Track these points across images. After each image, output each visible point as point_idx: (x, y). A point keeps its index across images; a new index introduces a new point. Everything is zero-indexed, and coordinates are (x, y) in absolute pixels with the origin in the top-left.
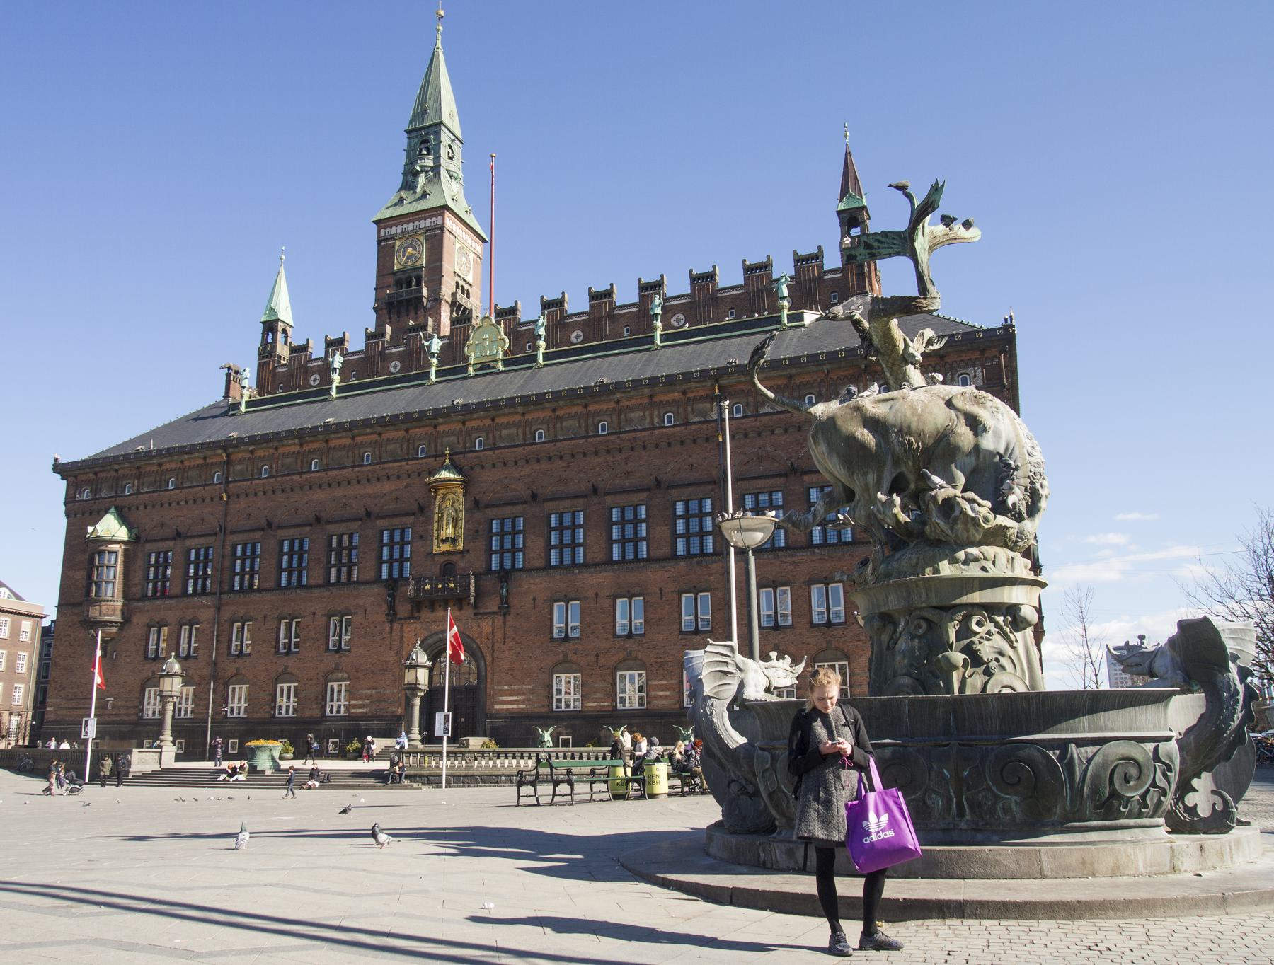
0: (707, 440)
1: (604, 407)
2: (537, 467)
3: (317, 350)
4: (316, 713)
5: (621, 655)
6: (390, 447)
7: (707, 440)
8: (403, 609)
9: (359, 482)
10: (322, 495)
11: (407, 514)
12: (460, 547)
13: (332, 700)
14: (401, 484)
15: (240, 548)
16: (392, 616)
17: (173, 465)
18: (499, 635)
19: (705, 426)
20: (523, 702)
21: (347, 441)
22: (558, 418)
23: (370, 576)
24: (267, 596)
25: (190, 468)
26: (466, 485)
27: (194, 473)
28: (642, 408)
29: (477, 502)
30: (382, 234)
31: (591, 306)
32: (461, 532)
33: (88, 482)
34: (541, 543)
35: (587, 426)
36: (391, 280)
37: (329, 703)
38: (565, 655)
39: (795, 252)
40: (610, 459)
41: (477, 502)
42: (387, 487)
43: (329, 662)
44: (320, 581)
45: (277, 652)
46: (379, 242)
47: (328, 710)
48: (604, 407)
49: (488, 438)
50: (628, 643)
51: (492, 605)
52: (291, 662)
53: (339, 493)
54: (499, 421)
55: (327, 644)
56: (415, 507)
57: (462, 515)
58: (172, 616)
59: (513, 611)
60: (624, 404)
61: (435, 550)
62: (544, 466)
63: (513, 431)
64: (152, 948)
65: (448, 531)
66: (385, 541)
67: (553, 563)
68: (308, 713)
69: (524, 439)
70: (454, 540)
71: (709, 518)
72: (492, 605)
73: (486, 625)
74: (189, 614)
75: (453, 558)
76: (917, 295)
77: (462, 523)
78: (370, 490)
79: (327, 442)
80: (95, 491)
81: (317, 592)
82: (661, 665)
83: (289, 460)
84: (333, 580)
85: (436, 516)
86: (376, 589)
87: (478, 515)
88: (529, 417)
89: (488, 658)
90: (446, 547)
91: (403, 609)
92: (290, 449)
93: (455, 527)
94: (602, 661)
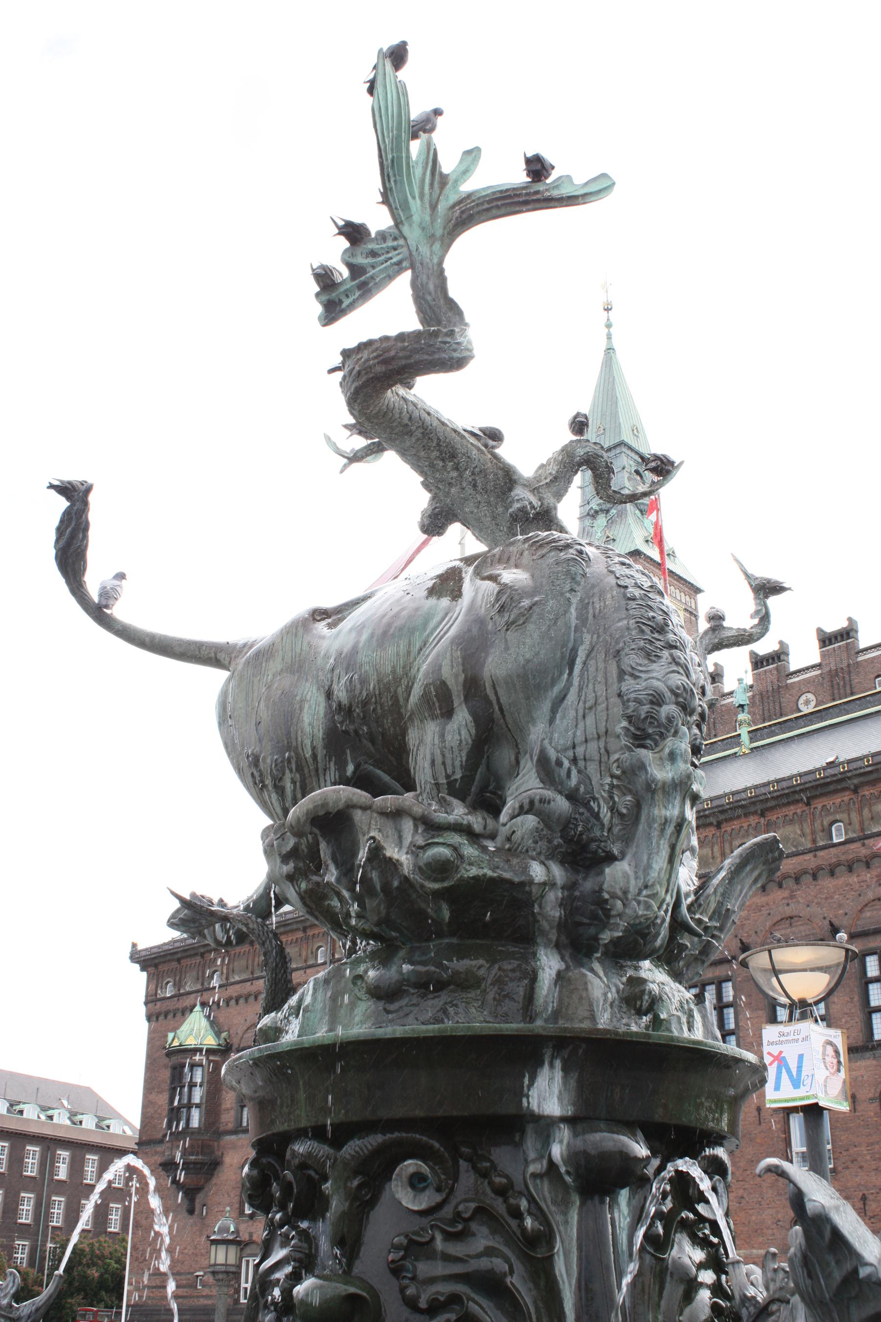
31: (823, 655)
35: (813, 832)
39: (820, 631)
40: (853, 879)
69: (814, 841)
71: (731, 1010)
76: (420, 327)
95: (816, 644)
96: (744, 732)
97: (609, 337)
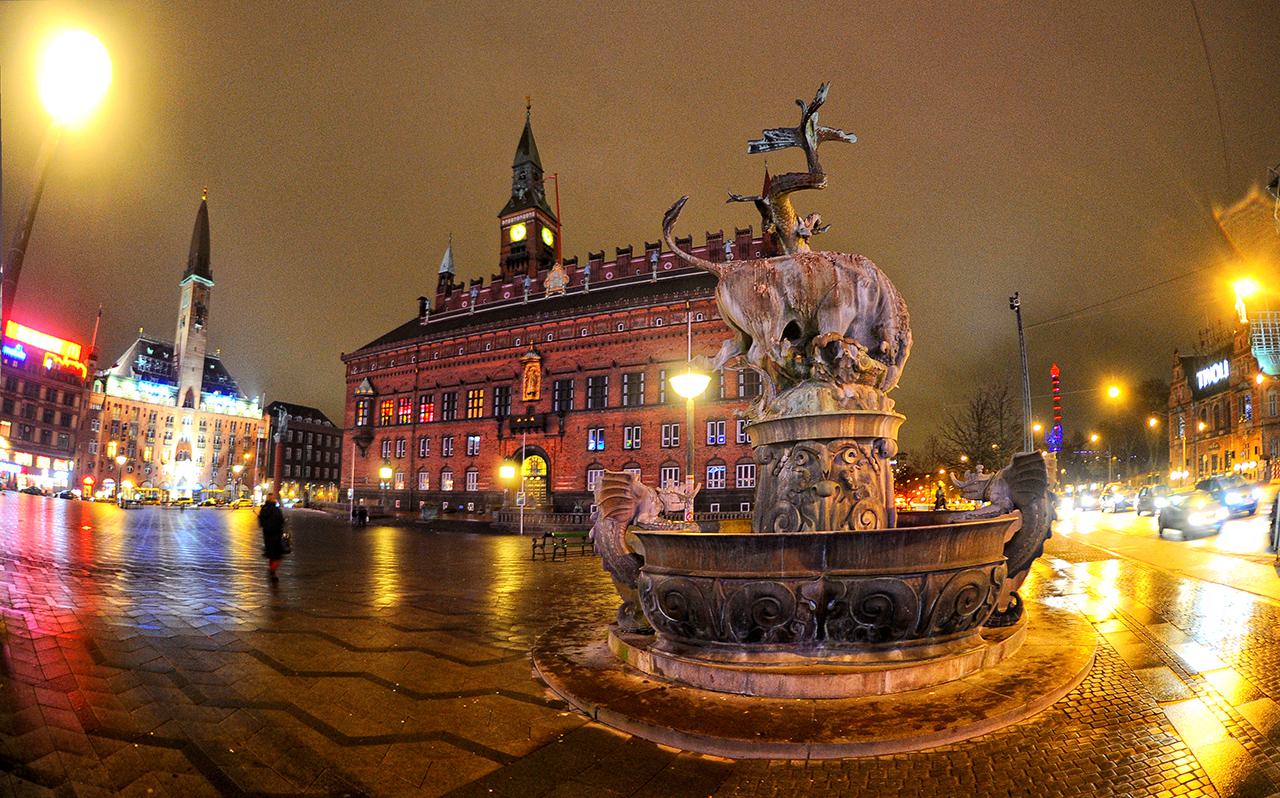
0: (681, 335)
1: (622, 314)
2: (582, 351)
3: (639, 251)
4: (461, 489)
5: (628, 460)
6: (501, 341)
7: (681, 335)
8: (506, 433)
9: (674, 335)
10: (464, 369)
11: (509, 379)
12: (537, 398)
13: (740, 477)
14: (505, 362)
15: (471, 393)
16: (500, 437)
17: (393, 353)
18: (558, 448)
19: (680, 327)
20: (571, 486)
21: (477, 337)
22: (613, 319)
23: (488, 414)
24: (437, 425)
25: (401, 355)
26: (541, 361)
27: (403, 357)
28: (645, 316)
29: (547, 372)
30: (504, 223)
32: (538, 388)
33: (356, 364)
34: (583, 394)
36: (509, 248)
37: (738, 479)
38: (595, 459)
41: (547, 372)
42: (498, 363)
43: (467, 462)
44: (463, 417)
45: (442, 456)
46: (502, 228)
47: (737, 484)
48: (622, 314)
49: (554, 335)
50: (632, 454)
51: (555, 431)
52: (448, 461)
53: (473, 367)
54: (561, 324)
55: (467, 451)
56: (575, 367)
57: (539, 379)
58: (393, 436)
59: (566, 434)
60: (633, 313)
61: (524, 399)
62: (586, 350)
63: (569, 330)
64: (905, 668)
65: (530, 389)
66: (497, 394)
67: (625, 404)
68: (458, 489)
70: (534, 394)
72: (555, 431)
73: (551, 443)
74: (446, 433)
75: (534, 403)
77: (539, 384)
78: (489, 365)
79: (467, 338)
80: (359, 369)
81: (462, 423)
82: (649, 466)
83: (447, 349)
84: (470, 416)
85: (525, 380)
86: (492, 421)
87: (548, 379)
88: (578, 321)
89: (552, 460)
90: (530, 397)
91: (506, 433)
92: (448, 343)
93: (535, 385)
94: (616, 463)
95: (615, 253)
96: (587, 285)
97: (528, 119)
